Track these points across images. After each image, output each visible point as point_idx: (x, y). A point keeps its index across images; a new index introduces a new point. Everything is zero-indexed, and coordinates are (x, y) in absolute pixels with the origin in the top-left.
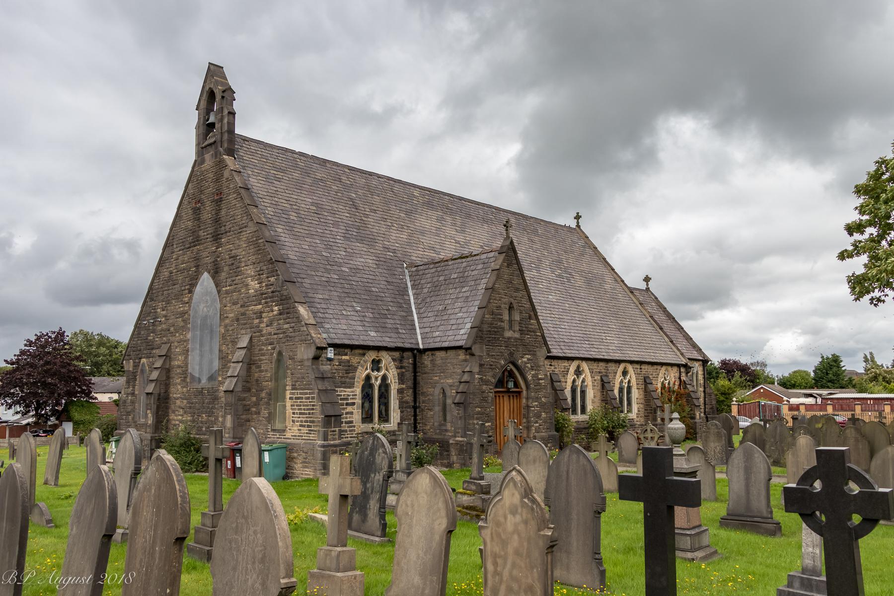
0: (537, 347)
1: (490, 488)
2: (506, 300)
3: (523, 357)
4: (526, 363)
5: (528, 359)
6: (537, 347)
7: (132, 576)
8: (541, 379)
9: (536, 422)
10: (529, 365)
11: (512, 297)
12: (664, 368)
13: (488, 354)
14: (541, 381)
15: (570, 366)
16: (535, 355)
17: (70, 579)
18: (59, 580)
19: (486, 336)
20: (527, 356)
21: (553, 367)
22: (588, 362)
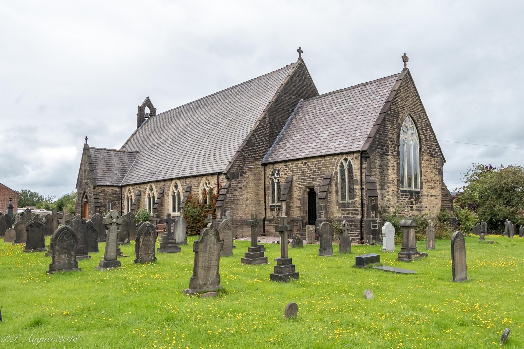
7: (77, 337)
10: (88, 192)
12: (204, 179)
17: (41, 339)
18: (34, 339)
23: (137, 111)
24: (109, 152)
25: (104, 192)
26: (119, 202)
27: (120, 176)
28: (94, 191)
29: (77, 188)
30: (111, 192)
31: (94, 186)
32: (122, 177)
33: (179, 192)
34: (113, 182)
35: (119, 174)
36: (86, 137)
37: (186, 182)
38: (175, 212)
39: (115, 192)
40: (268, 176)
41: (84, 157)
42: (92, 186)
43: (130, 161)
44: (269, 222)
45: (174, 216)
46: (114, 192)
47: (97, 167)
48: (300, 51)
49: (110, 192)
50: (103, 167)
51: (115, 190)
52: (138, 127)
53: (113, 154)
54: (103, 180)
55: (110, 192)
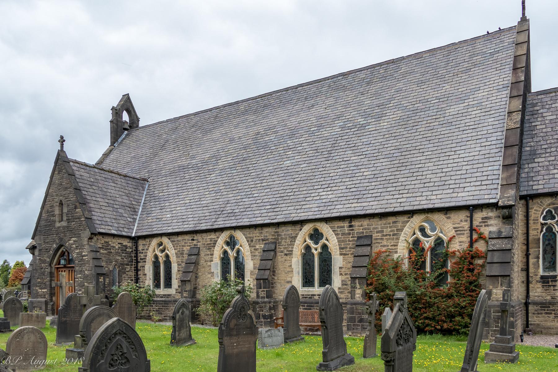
0: (81, 230)
1: (173, 337)
2: (57, 199)
3: (69, 240)
4: (72, 244)
5: (74, 241)
6: (81, 230)
8: (85, 256)
9: (80, 290)
10: (74, 246)
11: (61, 196)
13: (45, 242)
14: (84, 258)
15: (218, 237)
16: (80, 236)
19: (43, 229)
20: (73, 239)
21: (195, 242)
22: (244, 230)
23: (110, 116)
24: (102, 172)
25: (106, 246)
26: (131, 268)
27: (129, 219)
28: (90, 243)
29: (36, 238)
30: (119, 248)
31: (92, 234)
32: (132, 220)
33: (167, 256)
34: (121, 229)
35: (126, 216)
36: (62, 137)
37: (351, 226)
38: (160, 288)
39: (124, 248)
40: (537, 220)
41: (56, 176)
42: (87, 233)
43: (137, 194)
44: (541, 307)
45: (311, 293)
46: (124, 248)
47: (88, 197)
48: (62, 141)
49: (117, 247)
50: (99, 199)
51: (124, 244)
52: (113, 144)
53: (109, 177)
54: (103, 223)
55: (117, 247)
